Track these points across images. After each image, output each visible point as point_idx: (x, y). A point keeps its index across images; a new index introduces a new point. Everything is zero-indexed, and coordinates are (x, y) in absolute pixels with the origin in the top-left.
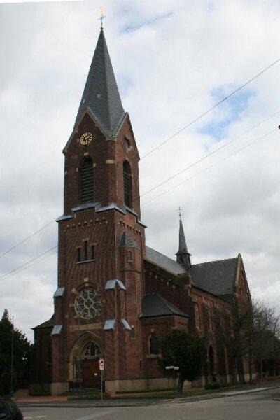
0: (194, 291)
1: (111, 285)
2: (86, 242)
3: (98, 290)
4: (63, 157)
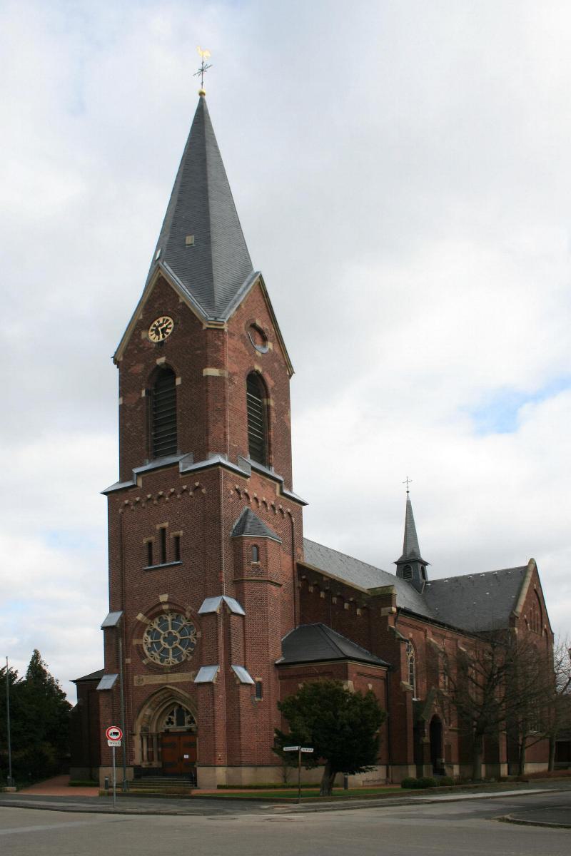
0: (402, 618)
1: (211, 605)
2: (163, 530)
3: (188, 614)
4: (115, 372)
